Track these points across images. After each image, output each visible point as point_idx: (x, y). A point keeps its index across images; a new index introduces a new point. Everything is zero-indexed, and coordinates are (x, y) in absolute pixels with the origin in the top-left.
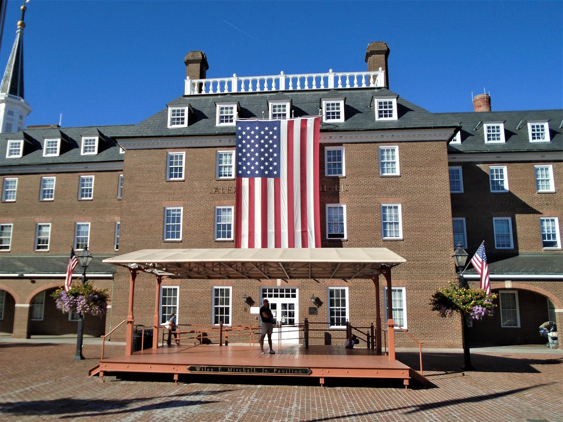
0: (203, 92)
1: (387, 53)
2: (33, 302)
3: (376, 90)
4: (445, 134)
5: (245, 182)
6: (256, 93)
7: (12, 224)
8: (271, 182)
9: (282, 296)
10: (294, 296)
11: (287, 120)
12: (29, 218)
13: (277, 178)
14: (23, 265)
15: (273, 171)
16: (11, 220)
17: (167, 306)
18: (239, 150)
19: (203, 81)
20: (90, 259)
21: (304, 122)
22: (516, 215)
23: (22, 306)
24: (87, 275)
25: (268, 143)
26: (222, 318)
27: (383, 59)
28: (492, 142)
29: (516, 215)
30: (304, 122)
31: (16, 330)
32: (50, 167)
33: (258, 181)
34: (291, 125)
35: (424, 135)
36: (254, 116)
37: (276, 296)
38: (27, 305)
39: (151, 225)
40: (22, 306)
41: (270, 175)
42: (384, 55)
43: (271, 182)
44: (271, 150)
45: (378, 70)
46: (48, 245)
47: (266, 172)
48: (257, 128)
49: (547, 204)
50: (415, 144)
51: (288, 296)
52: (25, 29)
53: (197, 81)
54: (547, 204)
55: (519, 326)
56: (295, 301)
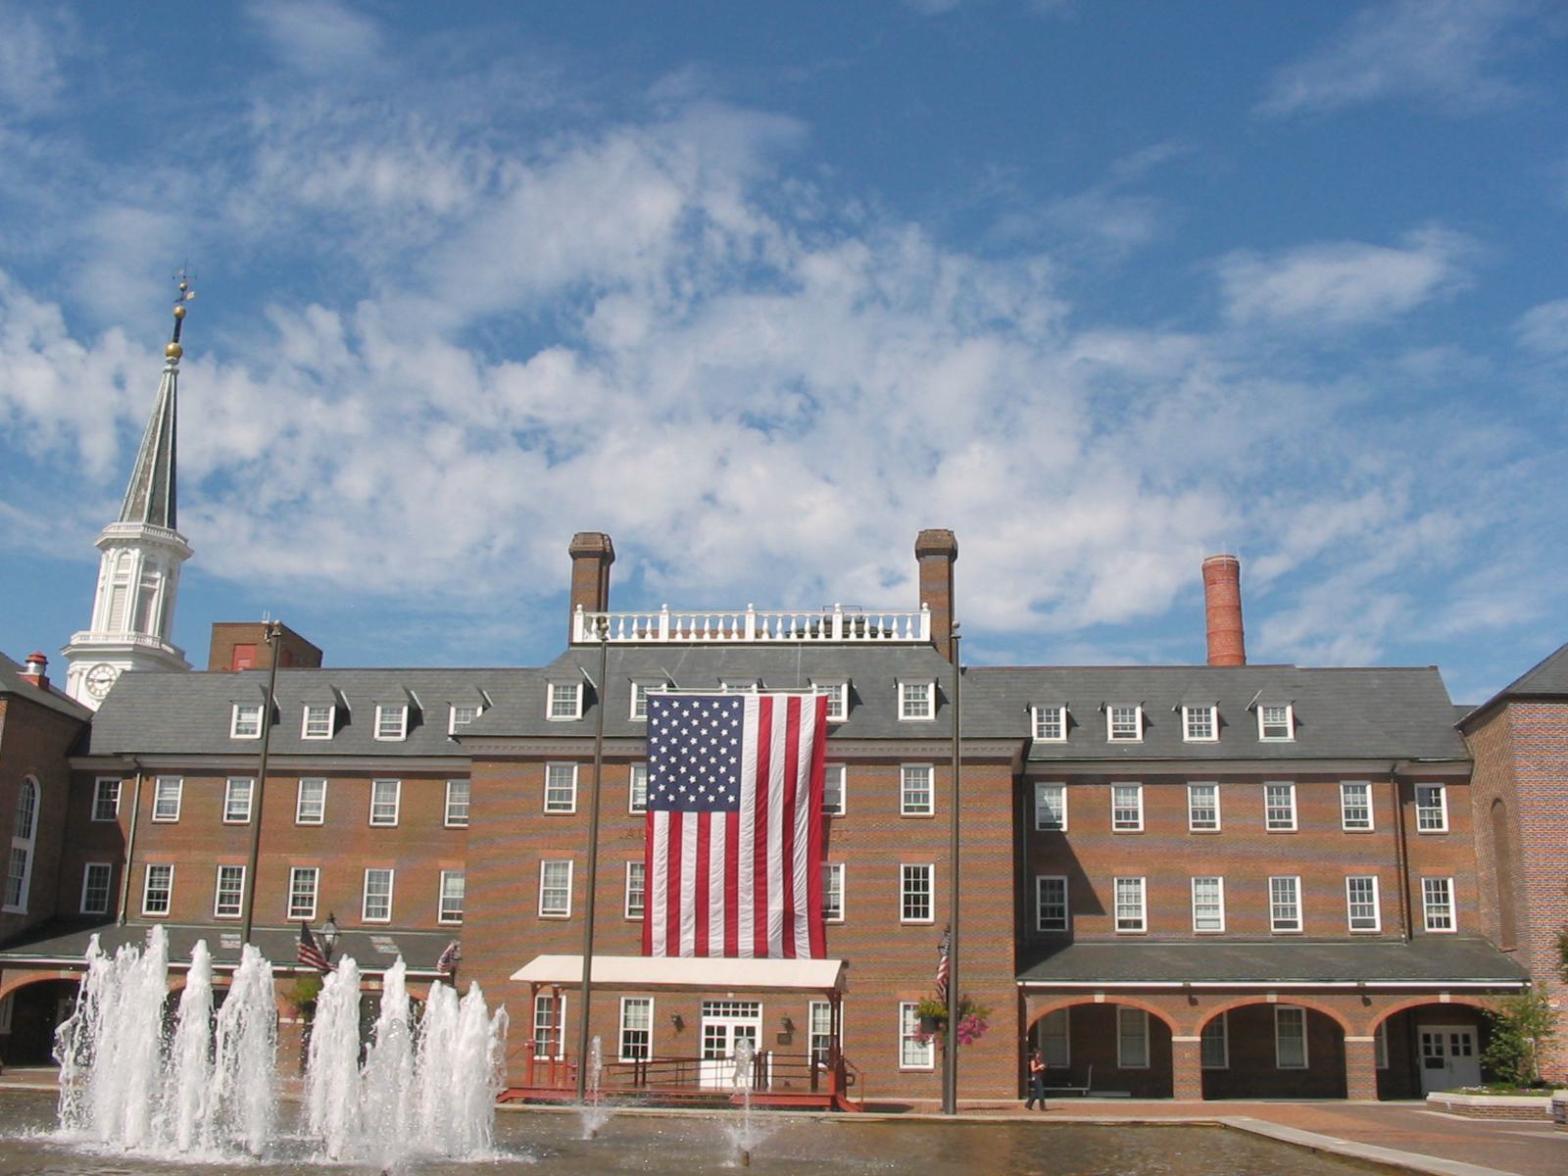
0: (822, 638)
5: (661, 818)
6: (688, 644)
8: (718, 819)
9: (735, 1014)
10: (755, 1014)
11: (815, 694)
13: (733, 811)
15: (726, 794)
17: (154, 900)
21: (794, 707)
22: (667, 813)
26: (636, 1049)
27: (945, 565)
28: (1196, 739)
29: (667, 813)
30: (794, 707)
34: (766, 706)
37: (726, 1014)
41: (721, 804)
42: (946, 557)
43: (718, 819)
44: (663, 750)
51: (745, 1014)
53: (595, 615)
54: (1207, 853)
55: (1148, 1065)
56: (757, 1023)
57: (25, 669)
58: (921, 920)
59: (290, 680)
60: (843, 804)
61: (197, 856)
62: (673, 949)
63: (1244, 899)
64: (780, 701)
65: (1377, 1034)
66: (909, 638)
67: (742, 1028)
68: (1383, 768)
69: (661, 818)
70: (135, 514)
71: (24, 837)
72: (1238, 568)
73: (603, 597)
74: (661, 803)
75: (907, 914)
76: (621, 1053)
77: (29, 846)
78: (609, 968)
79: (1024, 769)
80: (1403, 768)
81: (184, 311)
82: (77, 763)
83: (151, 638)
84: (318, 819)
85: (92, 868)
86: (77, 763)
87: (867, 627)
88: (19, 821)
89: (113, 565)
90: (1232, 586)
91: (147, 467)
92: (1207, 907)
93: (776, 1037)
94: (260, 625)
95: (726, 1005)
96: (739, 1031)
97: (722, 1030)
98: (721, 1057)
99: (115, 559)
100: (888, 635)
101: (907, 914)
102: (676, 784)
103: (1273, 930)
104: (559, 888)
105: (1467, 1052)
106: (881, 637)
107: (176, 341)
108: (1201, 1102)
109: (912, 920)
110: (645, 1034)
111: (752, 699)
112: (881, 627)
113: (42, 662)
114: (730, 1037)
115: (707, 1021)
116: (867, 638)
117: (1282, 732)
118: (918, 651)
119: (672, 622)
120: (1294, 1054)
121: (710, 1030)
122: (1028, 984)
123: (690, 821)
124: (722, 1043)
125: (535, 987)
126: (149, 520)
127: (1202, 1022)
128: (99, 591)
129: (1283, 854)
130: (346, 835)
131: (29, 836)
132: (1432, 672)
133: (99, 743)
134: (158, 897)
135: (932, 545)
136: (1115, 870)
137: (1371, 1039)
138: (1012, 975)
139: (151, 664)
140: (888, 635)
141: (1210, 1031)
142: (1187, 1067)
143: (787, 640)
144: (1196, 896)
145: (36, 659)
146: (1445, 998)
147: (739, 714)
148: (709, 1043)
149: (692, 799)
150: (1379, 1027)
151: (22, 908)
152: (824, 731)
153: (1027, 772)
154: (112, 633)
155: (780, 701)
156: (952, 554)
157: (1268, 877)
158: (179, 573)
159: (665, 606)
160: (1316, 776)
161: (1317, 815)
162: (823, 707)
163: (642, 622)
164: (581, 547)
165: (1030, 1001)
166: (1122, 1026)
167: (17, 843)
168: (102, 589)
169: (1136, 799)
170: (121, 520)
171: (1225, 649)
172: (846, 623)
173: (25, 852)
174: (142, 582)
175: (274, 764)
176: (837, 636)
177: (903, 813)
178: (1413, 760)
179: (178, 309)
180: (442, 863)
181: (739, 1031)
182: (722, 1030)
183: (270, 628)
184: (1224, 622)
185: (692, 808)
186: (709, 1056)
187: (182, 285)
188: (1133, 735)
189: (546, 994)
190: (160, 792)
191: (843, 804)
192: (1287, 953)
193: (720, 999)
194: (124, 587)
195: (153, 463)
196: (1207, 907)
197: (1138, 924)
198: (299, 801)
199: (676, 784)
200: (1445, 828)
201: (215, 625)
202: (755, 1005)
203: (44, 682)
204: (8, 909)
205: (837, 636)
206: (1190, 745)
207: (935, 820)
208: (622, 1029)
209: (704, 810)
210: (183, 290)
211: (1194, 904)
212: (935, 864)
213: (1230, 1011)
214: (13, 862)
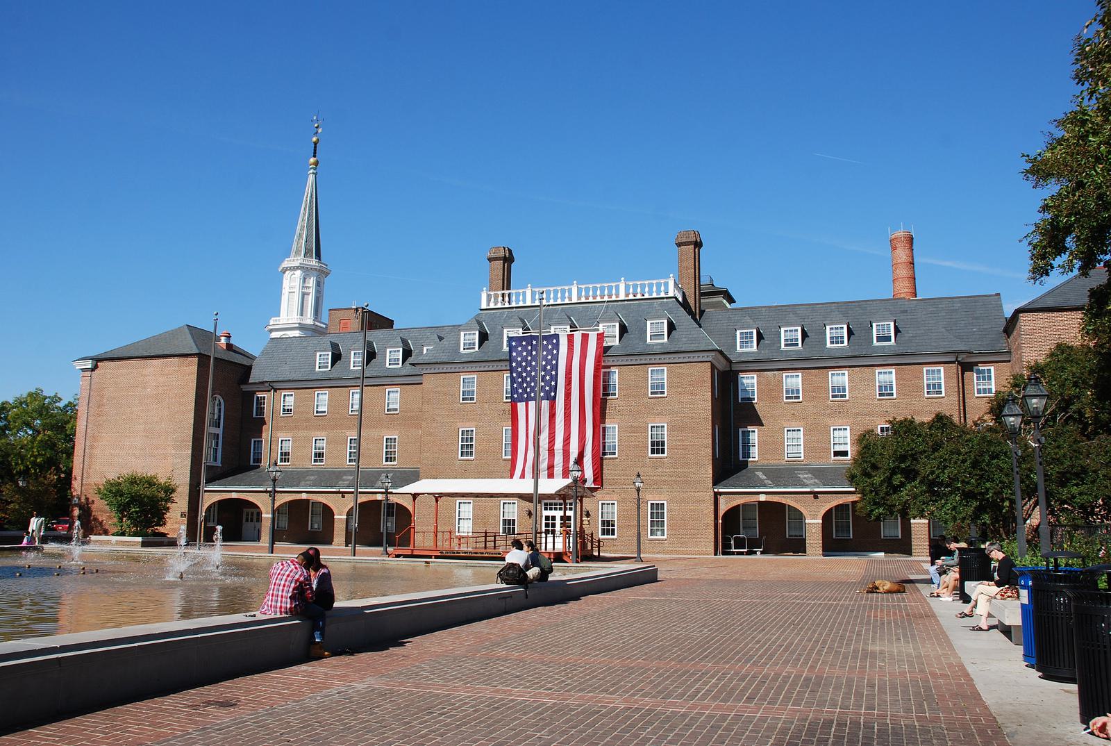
1: (698, 245)
2: (349, 514)
6: (512, 308)
7: (325, 438)
13: (553, 401)
14: (764, 477)
16: (323, 433)
18: (511, 370)
19: (507, 292)
20: (278, 474)
21: (585, 338)
23: (340, 517)
24: (277, 489)
30: (585, 338)
31: (336, 540)
32: (392, 379)
34: (571, 339)
35: (679, 358)
36: (367, 366)
37: (556, 509)
38: (345, 517)
42: (693, 246)
43: (545, 404)
48: (524, 343)
50: (682, 365)
52: (327, 280)
53: (500, 293)
57: (219, 340)
58: (660, 455)
59: (376, 336)
60: (756, 397)
61: (302, 433)
66: (663, 295)
67: (549, 516)
70: (298, 253)
71: (216, 427)
72: (912, 239)
73: (697, 274)
75: (653, 452)
79: (730, 367)
81: (318, 139)
82: (245, 388)
83: (309, 320)
85: (255, 441)
86: (245, 388)
89: (288, 281)
90: (907, 250)
91: (302, 227)
92: (841, 444)
94: (351, 309)
95: (556, 504)
97: (554, 518)
99: (289, 278)
101: (653, 452)
107: (315, 156)
108: (822, 557)
109: (655, 455)
110: (514, 520)
113: (229, 337)
115: (546, 513)
117: (888, 339)
118: (667, 302)
121: (547, 518)
122: (720, 490)
126: (305, 255)
127: (823, 512)
129: (887, 412)
131: (219, 427)
132: (996, 297)
133: (255, 376)
134: (285, 456)
135: (684, 240)
138: (711, 485)
139: (310, 333)
141: (827, 517)
142: (814, 538)
143: (643, 297)
144: (834, 437)
145: (225, 335)
147: (557, 346)
152: (603, 351)
153: (733, 369)
154: (289, 317)
157: (830, 427)
158: (324, 283)
159: (529, 285)
162: (601, 337)
165: (722, 499)
166: (789, 514)
171: (903, 288)
173: (218, 434)
174: (302, 289)
175: (359, 382)
177: (650, 395)
179: (314, 139)
182: (554, 518)
183: (357, 309)
184: (903, 272)
185: (532, 399)
187: (316, 125)
188: (797, 345)
190: (284, 401)
191: (756, 397)
193: (553, 502)
194: (294, 292)
195: (306, 225)
196: (841, 444)
198: (351, 402)
201: (330, 310)
203: (230, 347)
206: (831, 349)
207: (667, 399)
208: (502, 518)
209: (527, 401)
210: (317, 127)
211: (832, 443)
212: (667, 423)
213: (837, 507)
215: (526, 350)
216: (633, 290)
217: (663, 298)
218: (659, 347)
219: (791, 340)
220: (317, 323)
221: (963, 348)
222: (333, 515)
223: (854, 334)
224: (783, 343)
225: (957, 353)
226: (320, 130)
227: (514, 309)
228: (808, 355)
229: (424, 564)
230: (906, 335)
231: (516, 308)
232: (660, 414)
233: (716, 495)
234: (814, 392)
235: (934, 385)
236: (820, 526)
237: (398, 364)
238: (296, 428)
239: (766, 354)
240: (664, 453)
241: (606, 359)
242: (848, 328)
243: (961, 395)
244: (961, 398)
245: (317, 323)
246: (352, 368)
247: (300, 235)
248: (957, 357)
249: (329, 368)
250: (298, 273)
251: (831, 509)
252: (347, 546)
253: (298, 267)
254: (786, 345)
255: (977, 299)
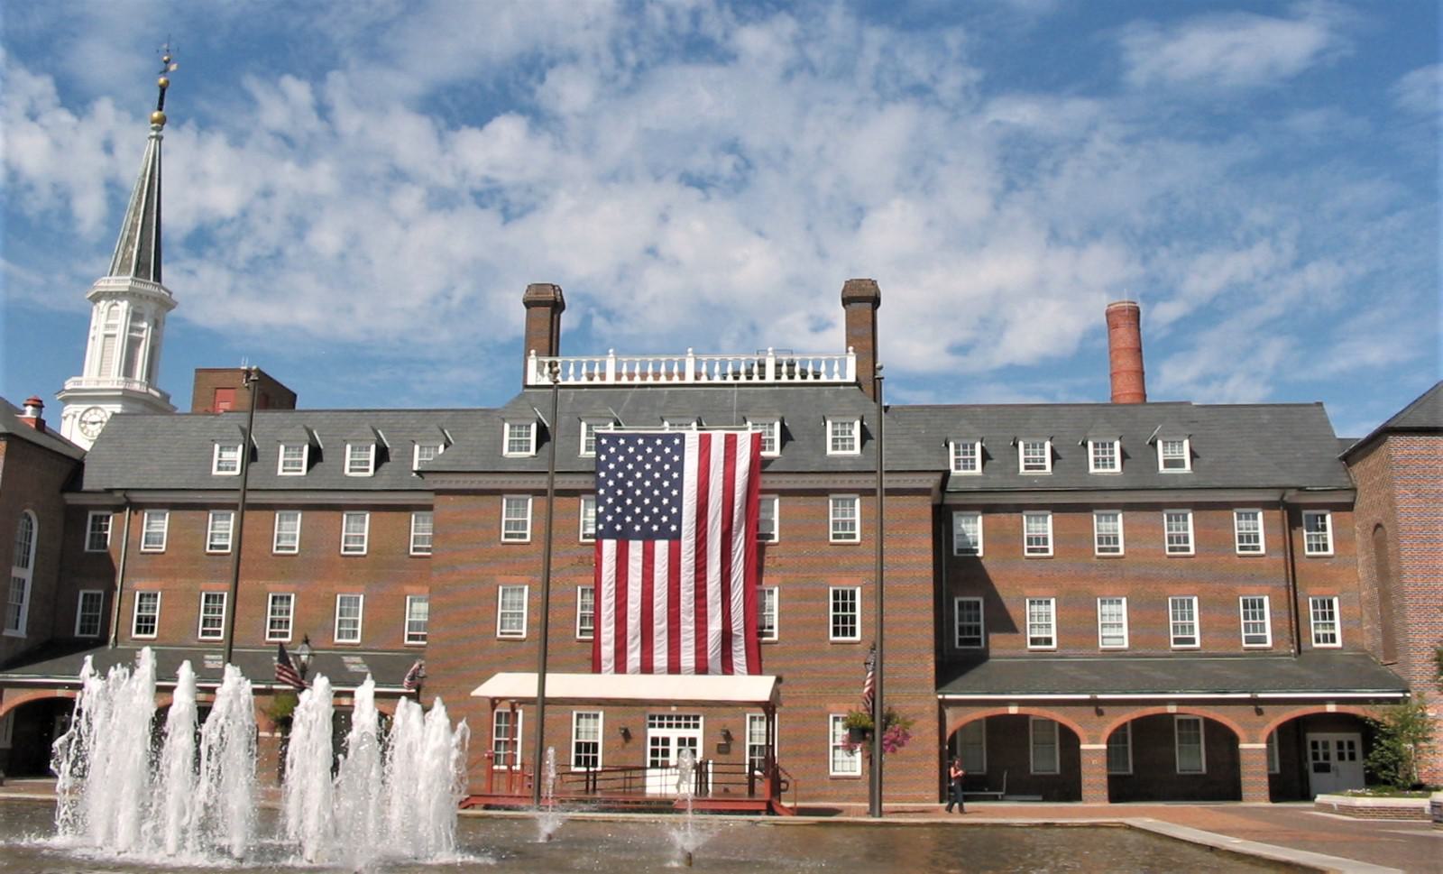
3: (842, 388)
4: (928, 481)
5: (609, 546)
8: (661, 547)
9: (678, 726)
10: (696, 726)
12: (255, 582)
13: (675, 539)
21: (731, 443)
23: (1093, 747)
25: (641, 515)
26: (587, 758)
27: (870, 312)
30: (731, 443)
31: (1086, 791)
33: (636, 548)
34: (705, 443)
37: (670, 726)
39: (478, 612)
40: (1093, 747)
43: (661, 547)
44: (647, 484)
45: (461, 863)
46: (290, 631)
47: (655, 528)
49: (1111, 576)
51: (687, 726)
53: (547, 360)
56: (698, 734)
59: (267, 421)
61: (183, 583)
62: (620, 667)
63: (1146, 617)
64: (718, 438)
65: (1269, 741)
68: (1273, 496)
69: (609, 546)
70: (123, 269)
71: (23, 566)
72: (1139, 313)
74: (609, 532)
75: (836, 633)
76: (573, 762)
77: (27, 575)
78: (561, 685)
79: (943, 498)
80: (1291, 497)
84: (293, 548)
85: (85, 595)
87: (797, 369)
88: (18, 552)
91: (134, 226)
92: (1112, 626)
93: (715, 747)
95: (670, 718)
96: (681, 741)
97: (666, 741)
98: (666, 766)
99: (106, 310)
100: (817, 376)
102: (623, 515)
103: (1173, 646)
104: (515, 610)
105: (1352, 757)
106: (810, 379)
107: (160, 109)
108: (1107, 804)
109: (840, 638)
110: (595, 745)
111: (692, 436)
112: (810, 369)
113: (38, 405)
114: (673, 747)
115: (652, 732)
116: (798, 379)
117: (1180, 464)
119: (618, 365)
120: (1192, 760)
121: (655, 741)
122: (948, 697)
123: (636, 548)
124: (666, 753)
125: (494, 702)
126: (137, 274)
127: (1108, 731)
128: (90, 340)
129: (1182, 576)
130: (319, 563)
131: (27, 566)
132: (1317, 408)
133: (91, 480)
135: (857, 294)
136: (1027, 592)
137: (1263, 746)
138: (932, 688)
139: (138, 407)
140: (817, 376)
141: (1116, 739)
142: (1094, 773)
143: (723, 382)
146: (1331, 708)
147: (680, 450)
148: (654, 753)
149: (637, 528)
150: (1271, 734)
151: (22, 632)
152: (759, 465)
153: (946, 502)
154: (102, 378)
155: (718, 438)
156: (876, 301)
157: (1167, 597)
158: (164, 323)
160: (1211, 504)
161: (1213, 541)
162: (758, 443)
163: (591, 365)
164: (534, 297)
165: (949, 713)
166: (1034, 735)
167: (17, 572)
168: (94, 338)
169: (1045, 526)
170: (111, 274)
171: (1127, 388)
172: (778, 366)
173: (24, 581)
176: (770, 378)
178: (1301, 489)
179: (162, 80)
180: (408, 588)
181: (681, 741)
182: (666, 741)
183: (248, 373)
184: (1126, 362)
185: (637, 536)
186: (654, 765)
187: (166, 58)
189: (504, 708)
192: (1185, 667)
194: (114, 336)
195: (140, 222)
196: (1112, 626)
197: (1048, 641)
199: (623, 515)
200: (1331, 551)
202: (696, 718)
203: (40, 424)
204: (8, 633)
205: (770, 378)
206: (1096, 476)
208: (574, 741)
209: (648, 538)
210: (166, 62)
211: (1100, 623)
213: (1134, 721)
214: (13, 590)
215: (625, 453)
216: (721, 368)
217: (732, 385)
218: (850, 462)
219: (1035, 460)
220: (151, 390)
221: (1294, 483)
222: (1079, 744)
223: (792, 440)
224: (1022, 465)
225: (1283, 489)
226: (173, 67)
227: (649, 389)
228: (1065, 484)
229: (746, 823)
230: (1206, 460)
231: (640, 386)
232: (850, 571)
233: (943, 704)
234: (1072, 543)
235: (844, 524)
236: (1104, 754)
237: (367, 470)
238: (171, 573)
239: (996, 481)
240: (1175, 643)
241: (768, 478)
242: (783, 426)
243: (1289, 554)
244: (1289, 557)
245: (151, 390)
246: (280, 473)
247: (130, 240)
248: (1283, 496)
249: (371, 472)
250: (123, 305)
251: (1124, 726)
252: (941, 802)
253: (124, 293)
254: (1027, 468)
255: (1291, 409)
